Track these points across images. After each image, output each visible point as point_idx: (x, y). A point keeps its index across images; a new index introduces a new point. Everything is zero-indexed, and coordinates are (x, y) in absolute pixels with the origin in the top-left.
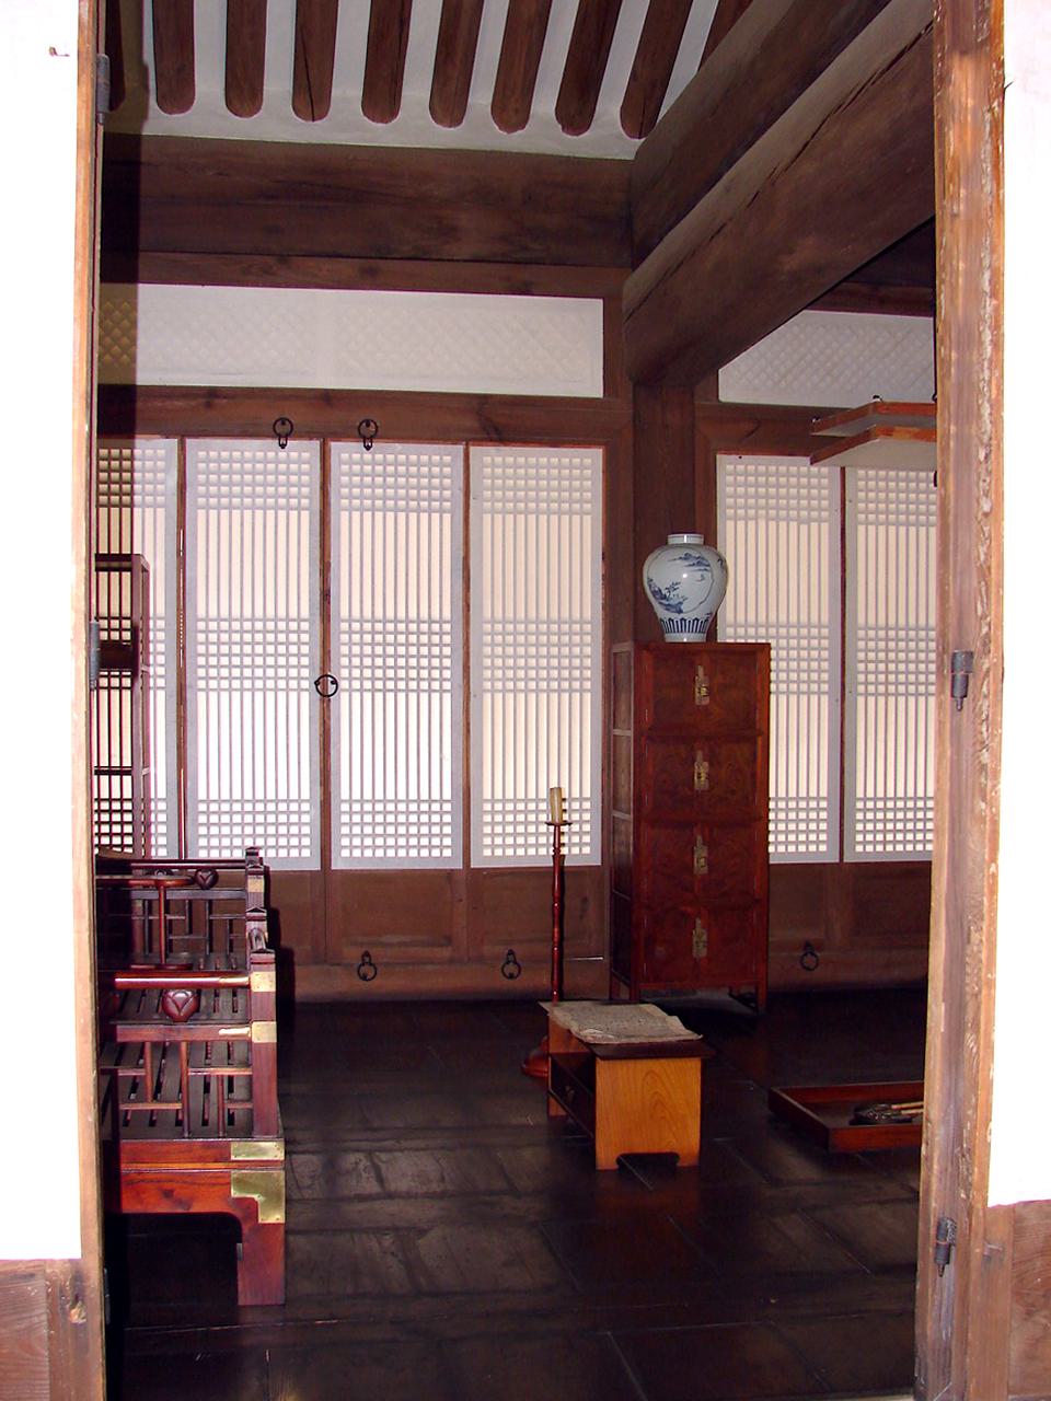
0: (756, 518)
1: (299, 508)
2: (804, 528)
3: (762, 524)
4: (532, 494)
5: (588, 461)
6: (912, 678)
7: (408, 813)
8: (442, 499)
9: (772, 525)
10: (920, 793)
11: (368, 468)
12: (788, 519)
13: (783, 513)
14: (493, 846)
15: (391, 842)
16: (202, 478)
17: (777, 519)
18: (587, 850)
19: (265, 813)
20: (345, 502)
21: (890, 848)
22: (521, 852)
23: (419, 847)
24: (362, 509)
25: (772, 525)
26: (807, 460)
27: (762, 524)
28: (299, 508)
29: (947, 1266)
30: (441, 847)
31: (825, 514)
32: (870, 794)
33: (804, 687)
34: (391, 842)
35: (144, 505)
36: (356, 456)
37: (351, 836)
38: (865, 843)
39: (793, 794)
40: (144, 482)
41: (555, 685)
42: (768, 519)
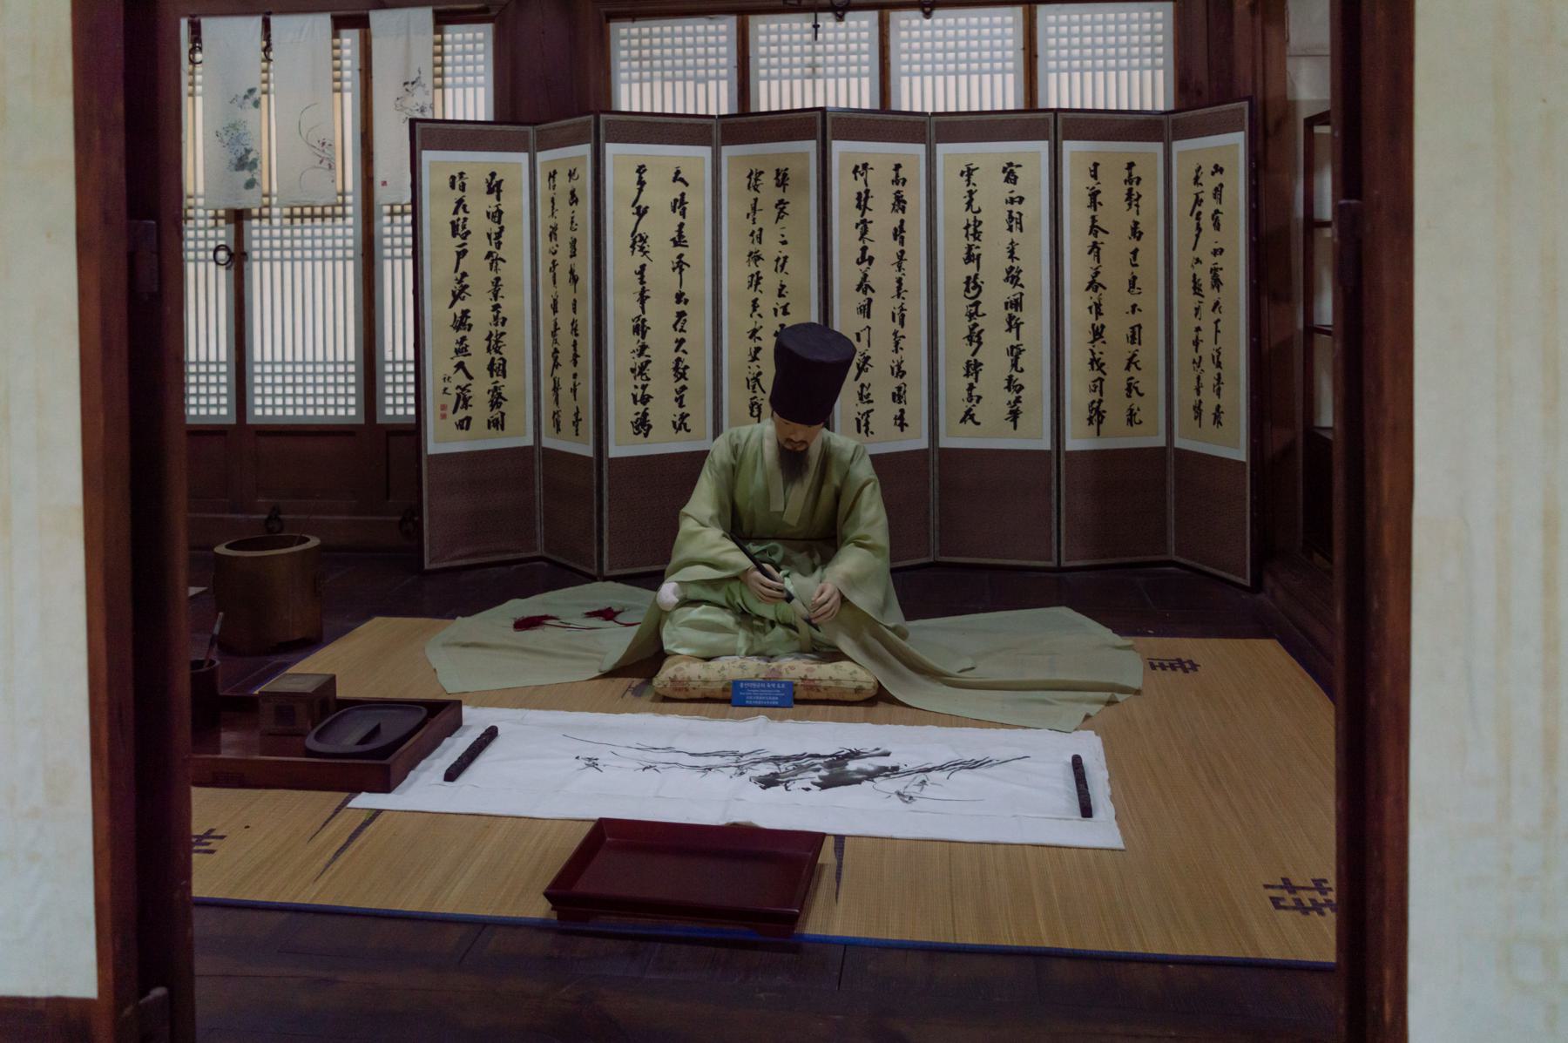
0: (651, 80)
1: (859, 75)
2: (701, 87)
3: (657, 85)
4: (1112, 51)
5: (865, 23)
6: (308, 243)
7: (325, 374)
8: (718, 67)
9: (668, 85)
10: (299, 358)
11: (1112, 28)
12: (685, 79)
13: (470, 79)
14: (395, 406)
15: (289, 401)
16: (905, 45)
17: (674, 80)
18: (352, 412)
19: (304, 374)
20: (1052, 64)
21: (321, 412)
22: (290, 412)
23: (325, 406)
24: (945, 73)
25: (668, 85)
26: (918, 13)
27: (657, 85)
28: (1004, 71)
29: (903, 768)
30: (346, 406)
31: (723, 72)
32: (268, 358)
33: (308, 254)
34: (320, 401)
35: (454, 86)
36: (916, 23)
37: (263, 396)
38: (198, 406)
39: (299, 358)
40: (454, 64)
41: (329, 253)
42: (663, 79)
